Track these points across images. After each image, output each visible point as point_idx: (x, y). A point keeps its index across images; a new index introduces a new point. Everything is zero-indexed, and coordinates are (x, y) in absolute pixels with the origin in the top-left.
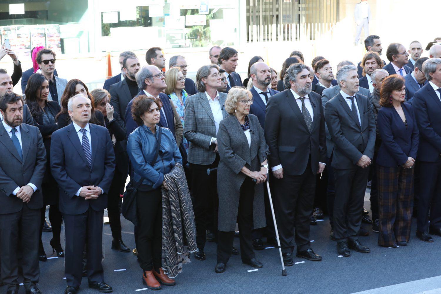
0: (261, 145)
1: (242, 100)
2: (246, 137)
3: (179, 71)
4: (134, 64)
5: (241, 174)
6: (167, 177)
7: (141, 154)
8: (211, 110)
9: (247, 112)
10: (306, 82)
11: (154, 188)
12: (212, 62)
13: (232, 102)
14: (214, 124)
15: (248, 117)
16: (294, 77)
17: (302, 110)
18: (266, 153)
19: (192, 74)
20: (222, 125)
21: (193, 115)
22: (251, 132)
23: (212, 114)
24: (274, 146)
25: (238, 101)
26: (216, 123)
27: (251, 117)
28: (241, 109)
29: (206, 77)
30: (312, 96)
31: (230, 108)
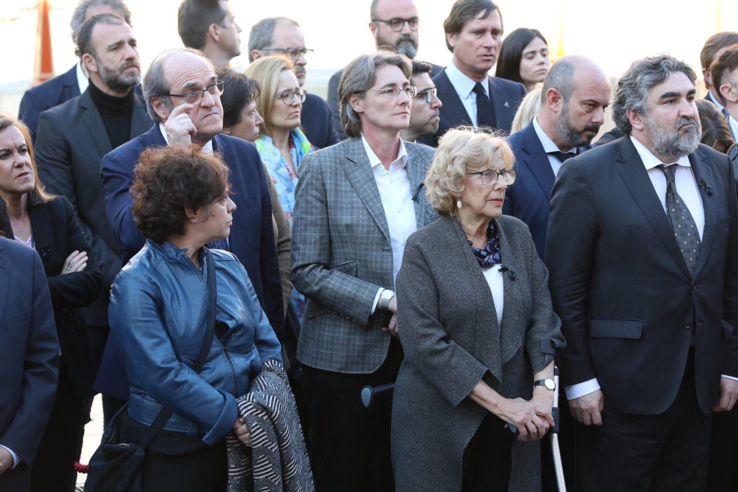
0: (536, 316)
1: (481, 170)
2: (489, 289)
3: (284, 69)
4: (117, 40)
5: (471, 405)
6: (246, 404)
7: (163, 335)
8: (380, 201)
9: (494, 210)
10: (679, 115)
11: (208, 442)
12: (381, 43)
13: (449, 175)
14: (389, 245)
15: (499, 224)
16: (641, 97)
17: (667, 206)
18: (552, 342)
19: (317, 83)
20: (414, 248)
21: (322, 212)
22: (506, 273)
23: (382, 214)
24: (576, 319)
25: (469, 173)
26: (396, 241)
27: (508, 228)
28: (476, 199)
29: (360, 93)
30: (704, 160)
31: (441, 194)
